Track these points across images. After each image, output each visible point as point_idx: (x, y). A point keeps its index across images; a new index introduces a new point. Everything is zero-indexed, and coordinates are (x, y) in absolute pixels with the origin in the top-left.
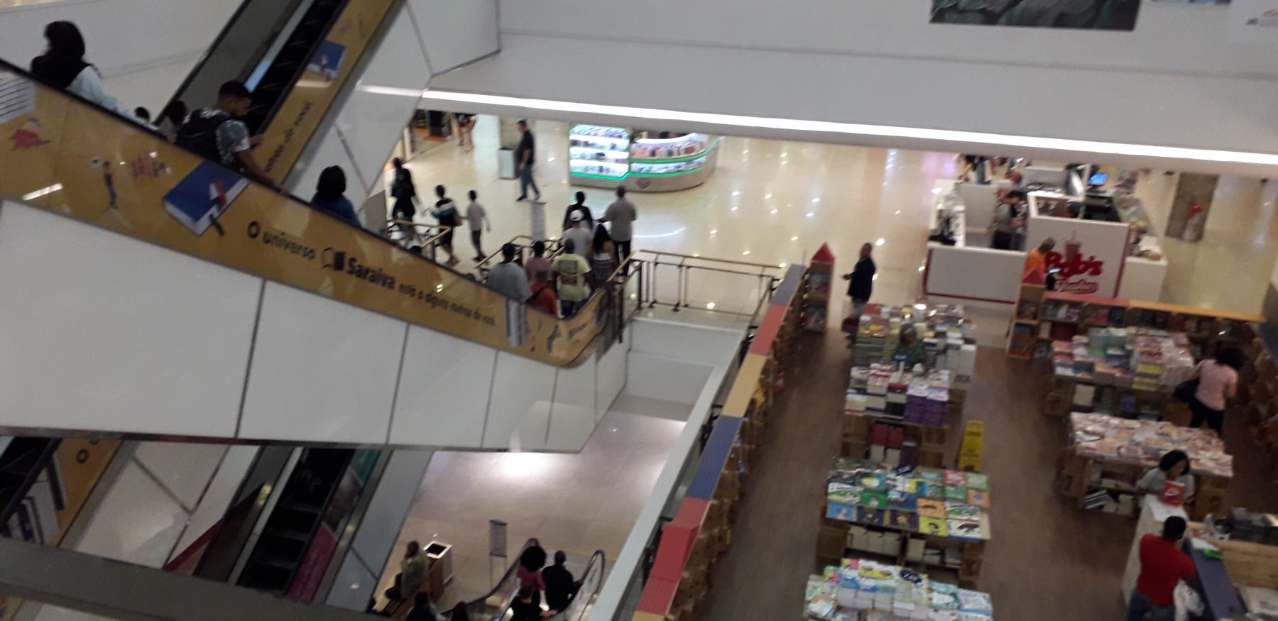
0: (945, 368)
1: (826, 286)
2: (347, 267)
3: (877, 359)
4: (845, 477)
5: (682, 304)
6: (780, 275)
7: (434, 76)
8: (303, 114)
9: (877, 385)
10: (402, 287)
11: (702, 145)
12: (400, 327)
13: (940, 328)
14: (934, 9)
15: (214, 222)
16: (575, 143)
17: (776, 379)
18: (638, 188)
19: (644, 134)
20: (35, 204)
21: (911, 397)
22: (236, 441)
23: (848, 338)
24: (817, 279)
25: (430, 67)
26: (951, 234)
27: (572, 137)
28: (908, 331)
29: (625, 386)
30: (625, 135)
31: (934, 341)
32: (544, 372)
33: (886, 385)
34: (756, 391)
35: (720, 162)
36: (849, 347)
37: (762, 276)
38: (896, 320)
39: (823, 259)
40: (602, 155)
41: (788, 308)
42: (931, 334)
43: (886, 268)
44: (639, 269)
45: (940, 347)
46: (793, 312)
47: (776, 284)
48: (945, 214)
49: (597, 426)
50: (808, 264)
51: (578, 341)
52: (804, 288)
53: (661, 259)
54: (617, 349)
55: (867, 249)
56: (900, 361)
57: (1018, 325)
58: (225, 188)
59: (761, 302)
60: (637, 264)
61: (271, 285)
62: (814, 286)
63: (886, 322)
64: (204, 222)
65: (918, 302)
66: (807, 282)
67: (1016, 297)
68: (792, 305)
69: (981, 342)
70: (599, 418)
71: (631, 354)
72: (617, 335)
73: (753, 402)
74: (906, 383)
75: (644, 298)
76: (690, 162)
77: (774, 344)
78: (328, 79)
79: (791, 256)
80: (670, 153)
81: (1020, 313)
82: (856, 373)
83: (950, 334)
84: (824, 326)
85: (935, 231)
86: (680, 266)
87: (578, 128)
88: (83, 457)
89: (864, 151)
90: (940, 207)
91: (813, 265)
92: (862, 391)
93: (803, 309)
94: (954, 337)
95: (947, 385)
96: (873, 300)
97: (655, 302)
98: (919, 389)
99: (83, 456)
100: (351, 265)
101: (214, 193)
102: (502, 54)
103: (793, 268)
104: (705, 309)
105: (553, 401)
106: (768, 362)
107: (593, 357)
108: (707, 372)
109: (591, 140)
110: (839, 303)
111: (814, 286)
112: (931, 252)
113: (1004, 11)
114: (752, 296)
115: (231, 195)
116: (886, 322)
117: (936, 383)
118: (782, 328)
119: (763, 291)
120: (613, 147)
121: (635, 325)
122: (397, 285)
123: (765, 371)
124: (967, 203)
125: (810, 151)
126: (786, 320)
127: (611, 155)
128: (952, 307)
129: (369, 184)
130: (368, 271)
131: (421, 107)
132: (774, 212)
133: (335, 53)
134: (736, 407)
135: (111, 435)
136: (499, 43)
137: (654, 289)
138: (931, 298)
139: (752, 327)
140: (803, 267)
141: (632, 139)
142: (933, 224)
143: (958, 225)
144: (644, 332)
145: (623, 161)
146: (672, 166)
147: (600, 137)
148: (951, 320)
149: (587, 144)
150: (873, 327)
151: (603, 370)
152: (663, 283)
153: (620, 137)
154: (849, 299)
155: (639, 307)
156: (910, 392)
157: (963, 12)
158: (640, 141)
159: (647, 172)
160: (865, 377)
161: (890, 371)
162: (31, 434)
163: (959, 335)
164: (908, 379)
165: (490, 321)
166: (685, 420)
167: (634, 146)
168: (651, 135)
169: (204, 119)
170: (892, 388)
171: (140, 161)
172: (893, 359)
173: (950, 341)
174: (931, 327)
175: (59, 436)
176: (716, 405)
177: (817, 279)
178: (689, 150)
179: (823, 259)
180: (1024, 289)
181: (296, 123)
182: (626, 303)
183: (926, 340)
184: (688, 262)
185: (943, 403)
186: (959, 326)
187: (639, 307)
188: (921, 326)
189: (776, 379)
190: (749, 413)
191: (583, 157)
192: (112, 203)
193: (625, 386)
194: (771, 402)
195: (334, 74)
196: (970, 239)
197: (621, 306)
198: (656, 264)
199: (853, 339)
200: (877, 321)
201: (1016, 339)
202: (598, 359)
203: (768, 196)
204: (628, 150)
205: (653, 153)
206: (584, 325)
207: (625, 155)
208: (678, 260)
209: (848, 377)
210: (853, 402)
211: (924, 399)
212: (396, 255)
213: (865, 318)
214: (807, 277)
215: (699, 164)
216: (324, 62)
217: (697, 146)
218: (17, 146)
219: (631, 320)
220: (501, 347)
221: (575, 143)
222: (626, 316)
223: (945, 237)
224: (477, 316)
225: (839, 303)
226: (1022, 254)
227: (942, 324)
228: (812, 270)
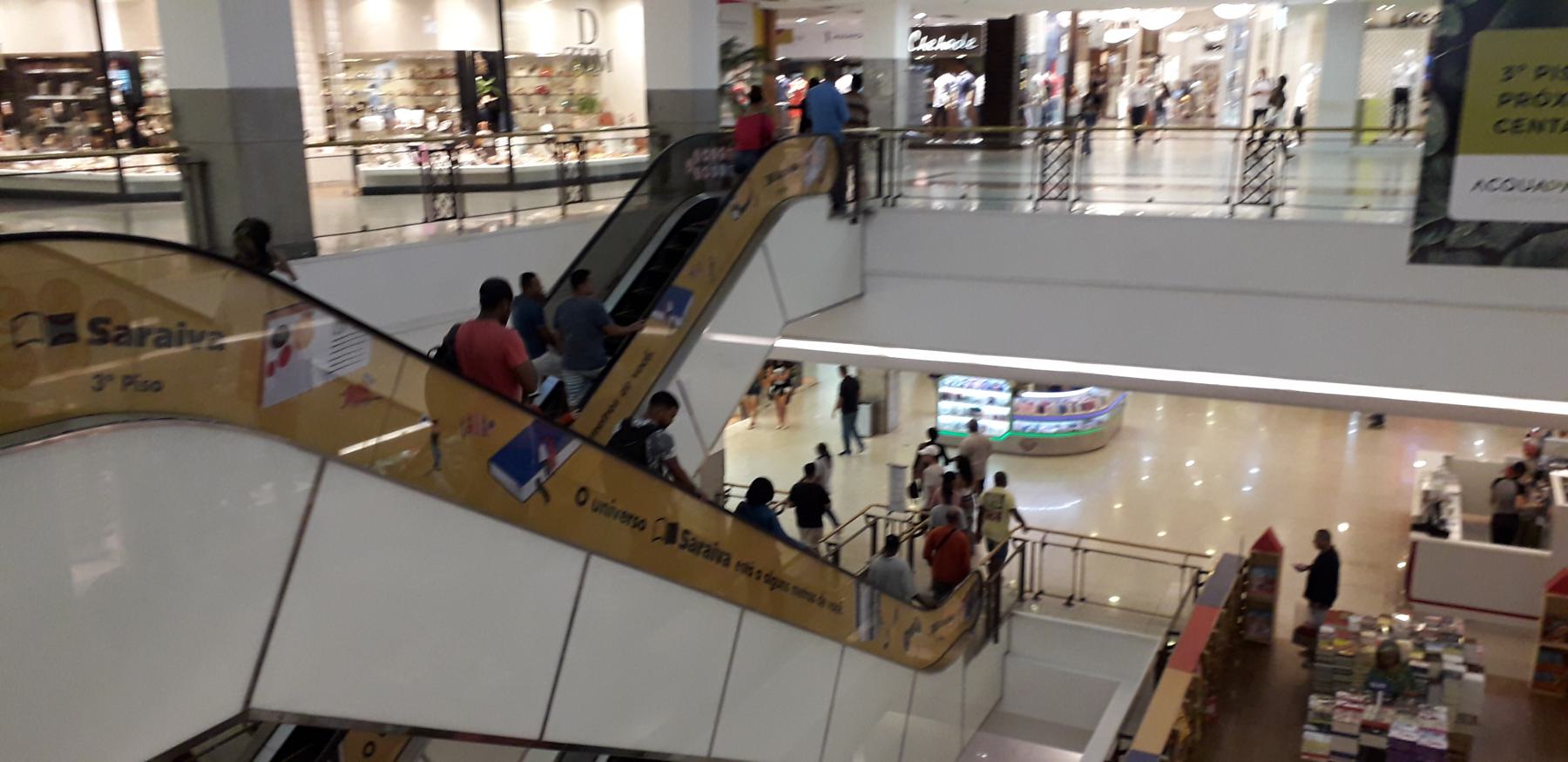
0: (1441, 703)
1: (1272, 584)
2: (679, 540)
3: (1345, 686)
4: (44, 85)
5: (1077, 596)
6: (1209, 566)
7: (788, 323)
8: (643, 365)
9: (1346, 721)
10: (738, 564)
11: (1104, 400)
12: (733, 612)
13: (1432, 649)
14: (1413, 247)
15: (540, 487)
16: (945, 397)
17: (1205, 704)
18: (1020, 450)
19: (1031, 386)
20: (353, 462)
21: (1394, 741)
22: (540, 744)
23: (1302, 654)
24: (1259, 575)
25: (784, 313)
26: (1443, 522)
27: (942, 390)
28: (1387, 649)
29: (1001, 699)
30: (1007, 387)
31: (1424, 665)
32: (893, 676)
33: (1358, 722)
34: (1179, 719)
35: (1128, 420)
36: (1304, 666)
37: (1184, 567)
38: (1370, 634)
39: (1267, 548)
40: (978, 410)
41: (1221, 611)
42: (1420, 655)
43: (1351, 563)
44: (1021, 550)
45: (1433, 674)
46: (1228, 615)
47: (1203, 578)
48: (1432, 497)
49: (963, 750)
50: (1246, 554)
51: (942, 638)
52: (1241, 586)
53: (1050, 538)
54: (991, 651)
55: (1323, 538)
56: (1375, 690)
57: (1543, 649)
58: (555, 447)
59: (1183, 601)
60: (1019, 543)
61: (595, 560)
62: (1256, 583)
63: (1356, 636)
64: (530, 486)
65: (1400, 611)
66: (1246, 577)
67: (1539, 609)
68: (1226, 606)
69: (1490, 670)
70: (967, 738)
71: (1010, 660)
72: (992, 632)
73: (1174, 735)
74: (1387, 721)
75: (1027, 587)
76: (1087, 419)
77: (1202, 657)
78: (672, 326)
79: (1223, 542)
80: (1063, 409)
81: (1546, 634)
82: (1316, 702)
83: (1446, 657)
84: (1269, 636)
85: (1419, 518)
86: (1075, 549)
87: (948, 380)
88: (369, 749)
89: (1319, 413)
90: (1426, 486)
91: (1253, 555)
92: (1325, 728)
93: (1240, 613)
94: (1452, 661)
95: (1445, 728)
96: (1338, 605)
97: (1041, 592)
98: (1405, 730)
99: (369, 749)
100: (685, 539)
101: (543, 454)
102: (866, 298)
103: (1226, 559)
104: (1107, 605)
105: (909, 712)
106: (1194, 681)
107: (960, 660)
108: (1112, 688)
109: (964, 392)
110: (1291, 603)
111: (1256, 583)
112: (1414, 545)
113: (1509, 250)
114: (1171, 591)
115: (562, 456)
116: (1356, 636)
117: (1429, 724)
118: (1213, 637)
119: (1187, 586)
120: (992, 401)
121: (1014, 620)
122: (733, 562)
123: (1191, 693)
124: (1462, 483)
125: (1246, 411)
126: (1218, 626)
127: (987, 410)
128: (1447, 620)
129: (708, 444)
130: (702, 545)
131: (773, 356)
132: (1198, 483)
133: (683, 297)
134: (1151, 738)
135: (398, 729)
136: (863, 285)
137: (1041, 576)
138: (1418, 607)
139: (1171, 634)
140: (1240, 558)
141: (1015, 392)
142: (1416, 510)
143: (1451, 512)
144: (1027, 629)
145: (1002, 418)
146: (1064, 425)
147: (976, 391)
148: (1448, 638)
149: (959, 398)
150: (1338, 642)
151: (973, 677)
152: (1054, 570)
153: (1000, 389)
154: (1305, 602)
155: (1021, 598)
156: (1393, 733)
157: (1453, 250)
158: (1025, 395)
159: (1033, 431)
160: (1328, 709)
161: (1365, 703)
162: (325, 724)
163: (1460, 659)
164: (1389, 716)
165: (836, 608)
166: (1079, 749)
167: (1017, 400)
168: (1038, 388)
169: (635, 428)
170: (1366, 727)
171: (470, 419)
172: (1367, 687)
173: (1447, 667)
174: (1420, 646)
175: (346, 727)
176: (1124, 735)
177: (1259, 575)
178: (1086, 406)
179: (1267, 548)
180: (1549, 600)
181: (635, 376)
182: (1004, 592)
183: (1413, 663)
184: (1085, 544)
185: (1441, 752)
186: (1459, 648)
187: (1021, 598)
188: (1405, 643)
189: (1205, 704)
190: (1169, 748)
191: (954, 413)
192: (436, 465)
193: (1001, 699)
194: (1198, 736)
195: (679, 322)
196: (1469, 530)
197: (997, 597)
198: (1044, 544)
199: (1311, 656)
200: (1344, 635)
201: (1541, 668)
202: (967, 661)
203: (1190, 463)
204: (1010, 404)
205: (1041, 409)
206: (950, 618)
207: (1006, 411)
208: (1073, 542)
209: (1304, 709)
210: (1314, 743)
211: (1413, 744)
212: (787, 555)
213: (1326, 629)
214: (1245, 571)
215: (1100, 423)
216: (670, 307)
217: (1098, 402)
218: (348, 402)
219: (1010, 615)
220: (836, 635)
221: (945, 397)
222: (1003, 609)
223: (1433, 525)
224: (822, 602)
225: (1291, 603)
226: (1546, 553)
227: (1437, 642)
228: (1251, 563)
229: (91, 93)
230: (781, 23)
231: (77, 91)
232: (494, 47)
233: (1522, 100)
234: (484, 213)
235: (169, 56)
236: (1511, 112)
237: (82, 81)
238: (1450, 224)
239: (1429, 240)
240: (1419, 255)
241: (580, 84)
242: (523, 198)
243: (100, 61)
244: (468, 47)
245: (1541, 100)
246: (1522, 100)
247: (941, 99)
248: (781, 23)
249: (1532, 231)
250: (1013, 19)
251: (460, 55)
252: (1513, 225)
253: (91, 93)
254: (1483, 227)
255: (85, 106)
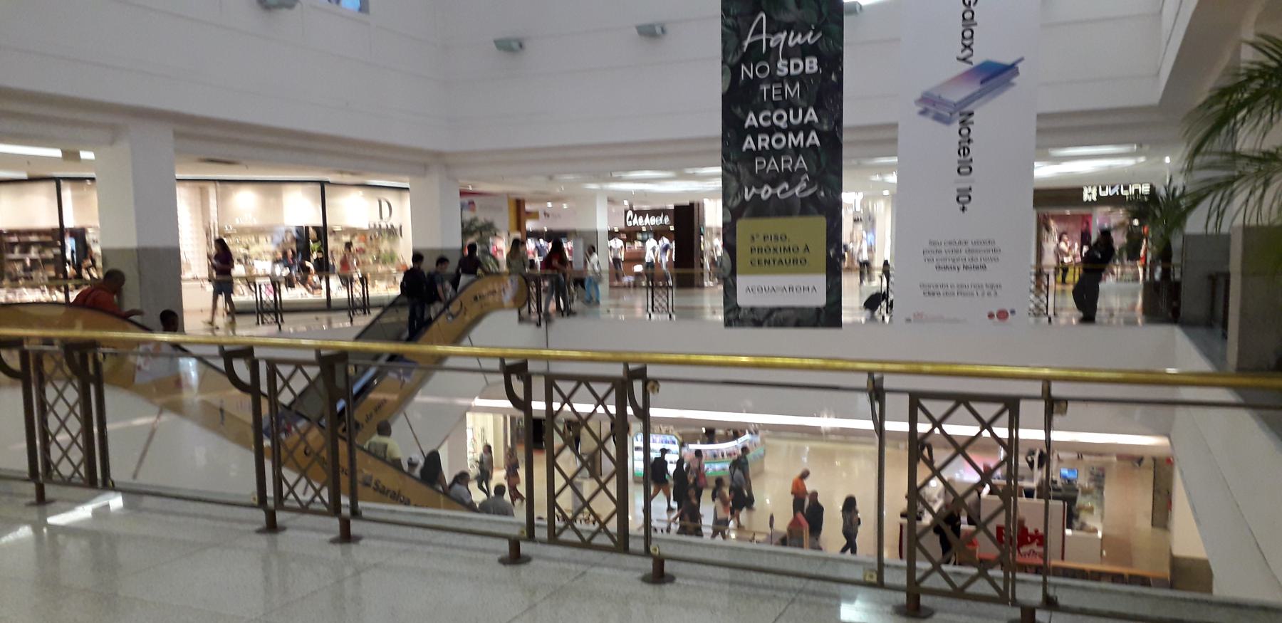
141: (682, 445)
229: (49, 254)
230: (528, 207)
231: (40, 252)
232: (320, 223)
233: (760, 250)
234: (292, 323)
235: (103, 230)
236: (756, 256)
237: (44, 245)
238: (738, 308)
239: (731, 316)
240: (728, 323)
241: (385, 246)
242: (333, 315)
243: (59, 233)
244: (303, 223)
245: (768, 250)
246: (760, 250)
247: (649, 256)
248: (528, 207)
249: (771, 311)
250: (692, 205)
251: (299, 230)
252: (764, 309)
253: (49, 254)
254: (752, 309)
255: (46, 261)
